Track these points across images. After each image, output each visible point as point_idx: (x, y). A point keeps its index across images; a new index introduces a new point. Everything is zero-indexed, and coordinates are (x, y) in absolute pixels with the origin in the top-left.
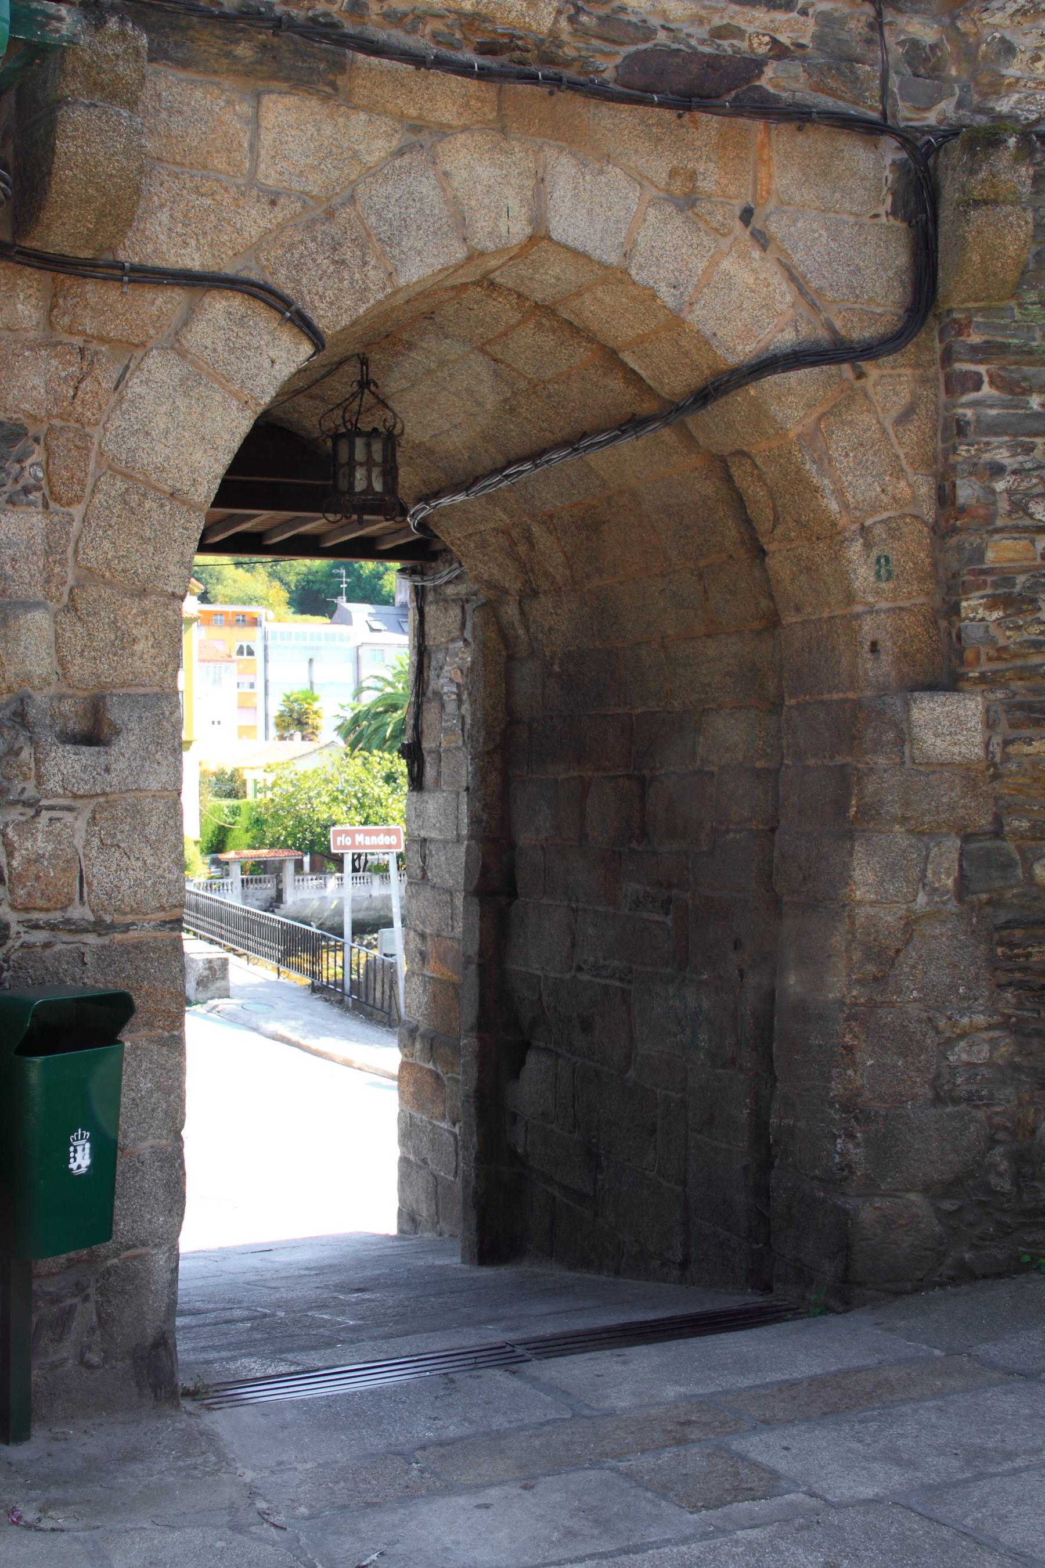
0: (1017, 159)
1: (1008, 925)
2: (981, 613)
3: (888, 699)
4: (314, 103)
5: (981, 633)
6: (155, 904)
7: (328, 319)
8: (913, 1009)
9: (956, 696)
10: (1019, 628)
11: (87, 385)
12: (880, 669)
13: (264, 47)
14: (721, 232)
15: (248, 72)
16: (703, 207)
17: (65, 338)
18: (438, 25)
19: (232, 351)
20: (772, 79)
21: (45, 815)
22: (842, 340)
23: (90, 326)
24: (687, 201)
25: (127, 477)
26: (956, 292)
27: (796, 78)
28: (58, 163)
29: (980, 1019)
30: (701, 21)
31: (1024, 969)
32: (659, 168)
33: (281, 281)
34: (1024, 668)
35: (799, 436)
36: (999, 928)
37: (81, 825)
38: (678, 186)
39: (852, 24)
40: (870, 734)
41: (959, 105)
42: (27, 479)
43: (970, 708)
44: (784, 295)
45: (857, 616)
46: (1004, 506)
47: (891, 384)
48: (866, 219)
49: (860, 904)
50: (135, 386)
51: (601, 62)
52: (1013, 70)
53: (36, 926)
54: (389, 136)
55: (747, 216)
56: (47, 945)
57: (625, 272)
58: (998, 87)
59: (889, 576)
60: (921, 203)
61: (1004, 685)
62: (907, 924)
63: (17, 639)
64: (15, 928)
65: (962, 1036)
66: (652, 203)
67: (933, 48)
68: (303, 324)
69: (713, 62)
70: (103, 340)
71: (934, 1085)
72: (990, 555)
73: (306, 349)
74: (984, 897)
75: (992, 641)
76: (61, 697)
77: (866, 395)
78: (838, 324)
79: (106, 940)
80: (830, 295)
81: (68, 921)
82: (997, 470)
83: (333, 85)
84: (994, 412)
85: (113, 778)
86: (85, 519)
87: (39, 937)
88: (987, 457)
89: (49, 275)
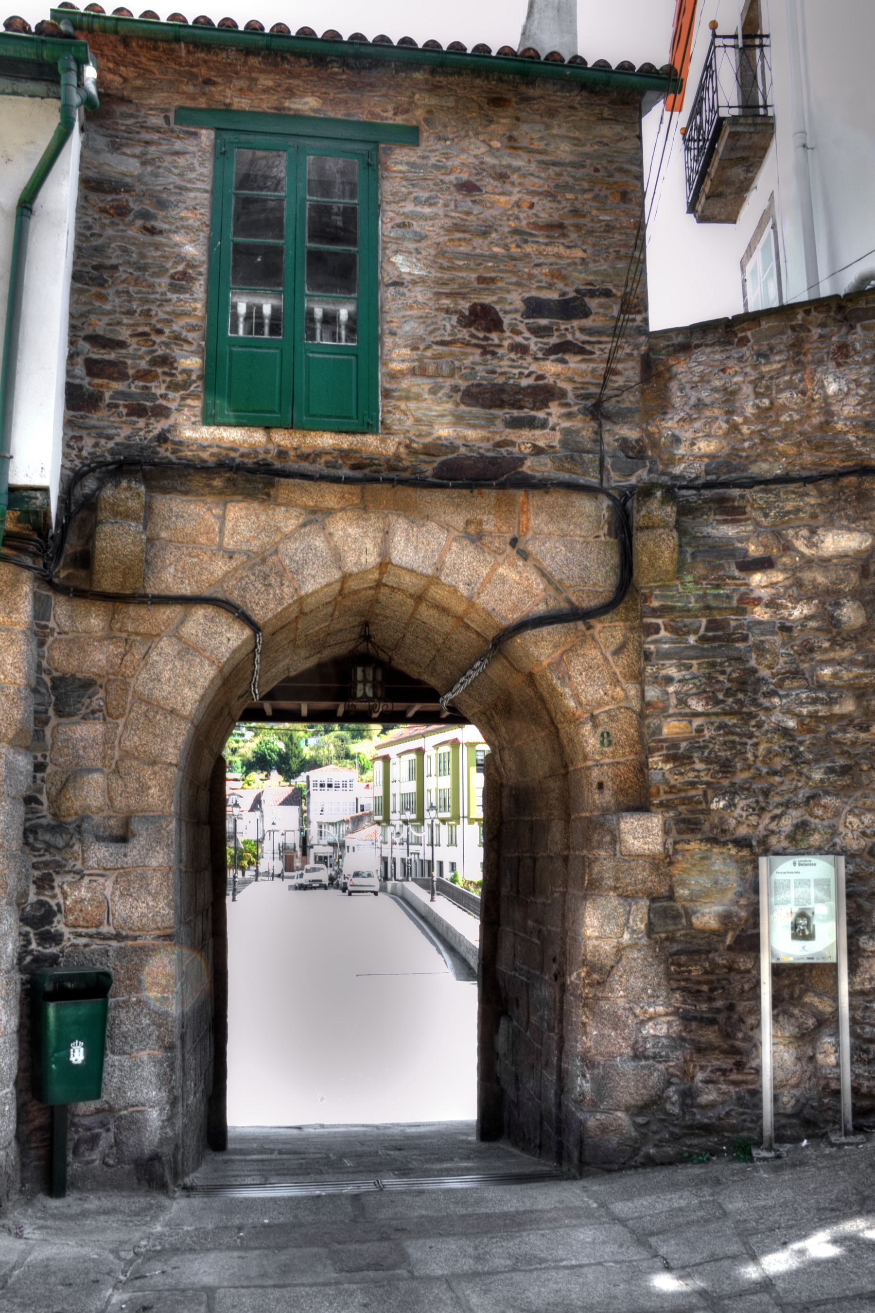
0: (663, 502)
1: (678, 953)
2: (660, 765)
3: (609, 817)
4: (256, 505)
5: (660, 777)
6: (153, 926)
7: (259, 615)
8: (621, 1002)
9: (646, 815)
10: (682, 774)
11: (128, 657)
12: (607, 798)
13: (228, 480)
14: (498, 552)
15: (221, 493)
16: (487, 540)
17: (118, 634)
18: (329, 458)
19: (206, 635)
20: (527, 467)
21: (86, 879)
22: (577, 608)
23: (130, 627)
24: (476, 537)
25: (148, 703)
26: (644, 579)
27: (546, 465)
28: (97, 552)
29: (661, 1009)
30: (488, 440)
31: (686, 980)
32: (458, 520)
33: (235, 597)
34: (684, 798)
35: (550, 664)
36: (671, 955)
37: (109, 884)
38: (472, 529)
39: (584, 433)
40: (596, 837)
41: (650, 471)
42: (95, 705)
43: (655, 822)
44: (538, 585)
45: (589, 768)
46: (673, 701)
47: (610, 631)
48: (591, 539)
49: (589, 938)
50: (154, 656)
51: (424, 467)
52: (681, 451)
53: (80, 935)
54: (298, 517)
55: (514, 542)
56: (86, 946)
57: (438, 578)
58: (672, 461)
59: (610, 743)
60: (623, 529)
61: (675, 808)
62: (618, 951)
63: (82, 789)
64: (66, 936)
65: (650, 1019)
66: (455, 540)
67: (637, 441)
68: (245, 618)
69: (493, 461)
70: (137, 634)
71: (634, 1048)
72: (665, 730)
73: (247, 632)
74: (663, 935)
75: (666, 782)
76: (110, 817)
77: (593, 639)
78: (574, 599)
79: (123, 944)
80: (567, 583)
81: (99, 934)
82: (669, 680)
83: (268, 495)
84: (666, 646)
85: (129, 860)
86: (125, 726)
87: (84, 941)
88: (664, 672)
89: (110, 604)
